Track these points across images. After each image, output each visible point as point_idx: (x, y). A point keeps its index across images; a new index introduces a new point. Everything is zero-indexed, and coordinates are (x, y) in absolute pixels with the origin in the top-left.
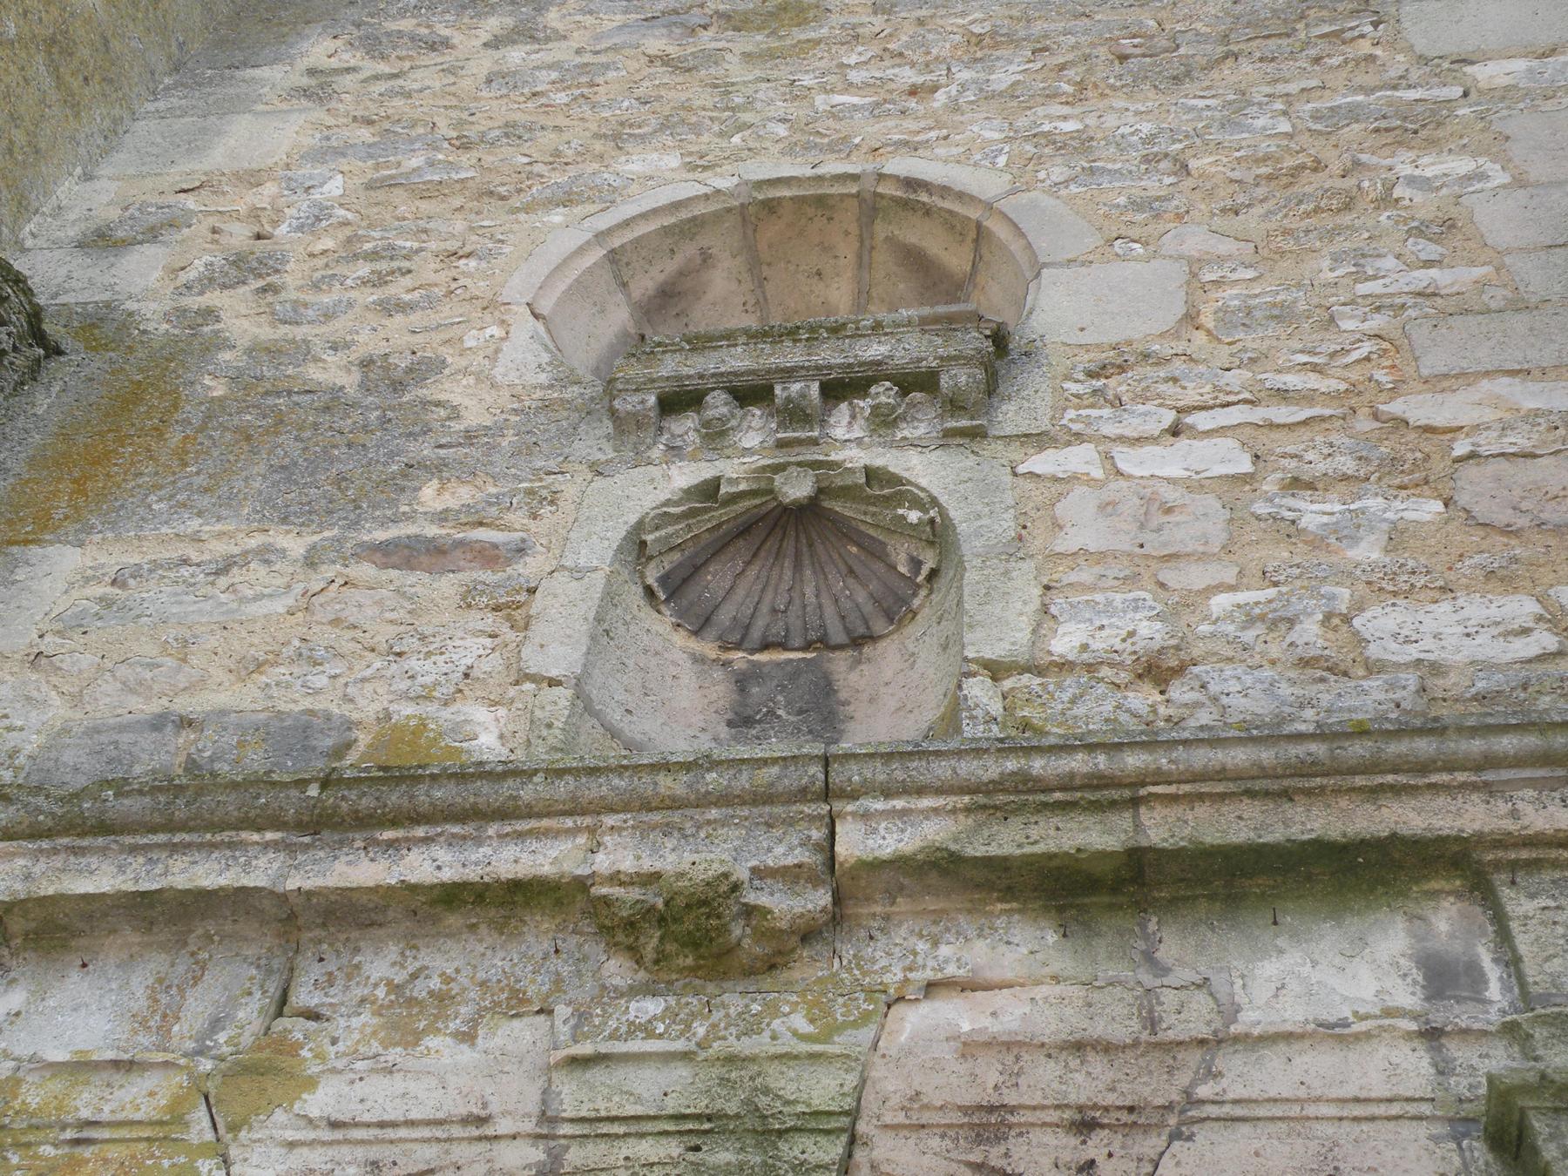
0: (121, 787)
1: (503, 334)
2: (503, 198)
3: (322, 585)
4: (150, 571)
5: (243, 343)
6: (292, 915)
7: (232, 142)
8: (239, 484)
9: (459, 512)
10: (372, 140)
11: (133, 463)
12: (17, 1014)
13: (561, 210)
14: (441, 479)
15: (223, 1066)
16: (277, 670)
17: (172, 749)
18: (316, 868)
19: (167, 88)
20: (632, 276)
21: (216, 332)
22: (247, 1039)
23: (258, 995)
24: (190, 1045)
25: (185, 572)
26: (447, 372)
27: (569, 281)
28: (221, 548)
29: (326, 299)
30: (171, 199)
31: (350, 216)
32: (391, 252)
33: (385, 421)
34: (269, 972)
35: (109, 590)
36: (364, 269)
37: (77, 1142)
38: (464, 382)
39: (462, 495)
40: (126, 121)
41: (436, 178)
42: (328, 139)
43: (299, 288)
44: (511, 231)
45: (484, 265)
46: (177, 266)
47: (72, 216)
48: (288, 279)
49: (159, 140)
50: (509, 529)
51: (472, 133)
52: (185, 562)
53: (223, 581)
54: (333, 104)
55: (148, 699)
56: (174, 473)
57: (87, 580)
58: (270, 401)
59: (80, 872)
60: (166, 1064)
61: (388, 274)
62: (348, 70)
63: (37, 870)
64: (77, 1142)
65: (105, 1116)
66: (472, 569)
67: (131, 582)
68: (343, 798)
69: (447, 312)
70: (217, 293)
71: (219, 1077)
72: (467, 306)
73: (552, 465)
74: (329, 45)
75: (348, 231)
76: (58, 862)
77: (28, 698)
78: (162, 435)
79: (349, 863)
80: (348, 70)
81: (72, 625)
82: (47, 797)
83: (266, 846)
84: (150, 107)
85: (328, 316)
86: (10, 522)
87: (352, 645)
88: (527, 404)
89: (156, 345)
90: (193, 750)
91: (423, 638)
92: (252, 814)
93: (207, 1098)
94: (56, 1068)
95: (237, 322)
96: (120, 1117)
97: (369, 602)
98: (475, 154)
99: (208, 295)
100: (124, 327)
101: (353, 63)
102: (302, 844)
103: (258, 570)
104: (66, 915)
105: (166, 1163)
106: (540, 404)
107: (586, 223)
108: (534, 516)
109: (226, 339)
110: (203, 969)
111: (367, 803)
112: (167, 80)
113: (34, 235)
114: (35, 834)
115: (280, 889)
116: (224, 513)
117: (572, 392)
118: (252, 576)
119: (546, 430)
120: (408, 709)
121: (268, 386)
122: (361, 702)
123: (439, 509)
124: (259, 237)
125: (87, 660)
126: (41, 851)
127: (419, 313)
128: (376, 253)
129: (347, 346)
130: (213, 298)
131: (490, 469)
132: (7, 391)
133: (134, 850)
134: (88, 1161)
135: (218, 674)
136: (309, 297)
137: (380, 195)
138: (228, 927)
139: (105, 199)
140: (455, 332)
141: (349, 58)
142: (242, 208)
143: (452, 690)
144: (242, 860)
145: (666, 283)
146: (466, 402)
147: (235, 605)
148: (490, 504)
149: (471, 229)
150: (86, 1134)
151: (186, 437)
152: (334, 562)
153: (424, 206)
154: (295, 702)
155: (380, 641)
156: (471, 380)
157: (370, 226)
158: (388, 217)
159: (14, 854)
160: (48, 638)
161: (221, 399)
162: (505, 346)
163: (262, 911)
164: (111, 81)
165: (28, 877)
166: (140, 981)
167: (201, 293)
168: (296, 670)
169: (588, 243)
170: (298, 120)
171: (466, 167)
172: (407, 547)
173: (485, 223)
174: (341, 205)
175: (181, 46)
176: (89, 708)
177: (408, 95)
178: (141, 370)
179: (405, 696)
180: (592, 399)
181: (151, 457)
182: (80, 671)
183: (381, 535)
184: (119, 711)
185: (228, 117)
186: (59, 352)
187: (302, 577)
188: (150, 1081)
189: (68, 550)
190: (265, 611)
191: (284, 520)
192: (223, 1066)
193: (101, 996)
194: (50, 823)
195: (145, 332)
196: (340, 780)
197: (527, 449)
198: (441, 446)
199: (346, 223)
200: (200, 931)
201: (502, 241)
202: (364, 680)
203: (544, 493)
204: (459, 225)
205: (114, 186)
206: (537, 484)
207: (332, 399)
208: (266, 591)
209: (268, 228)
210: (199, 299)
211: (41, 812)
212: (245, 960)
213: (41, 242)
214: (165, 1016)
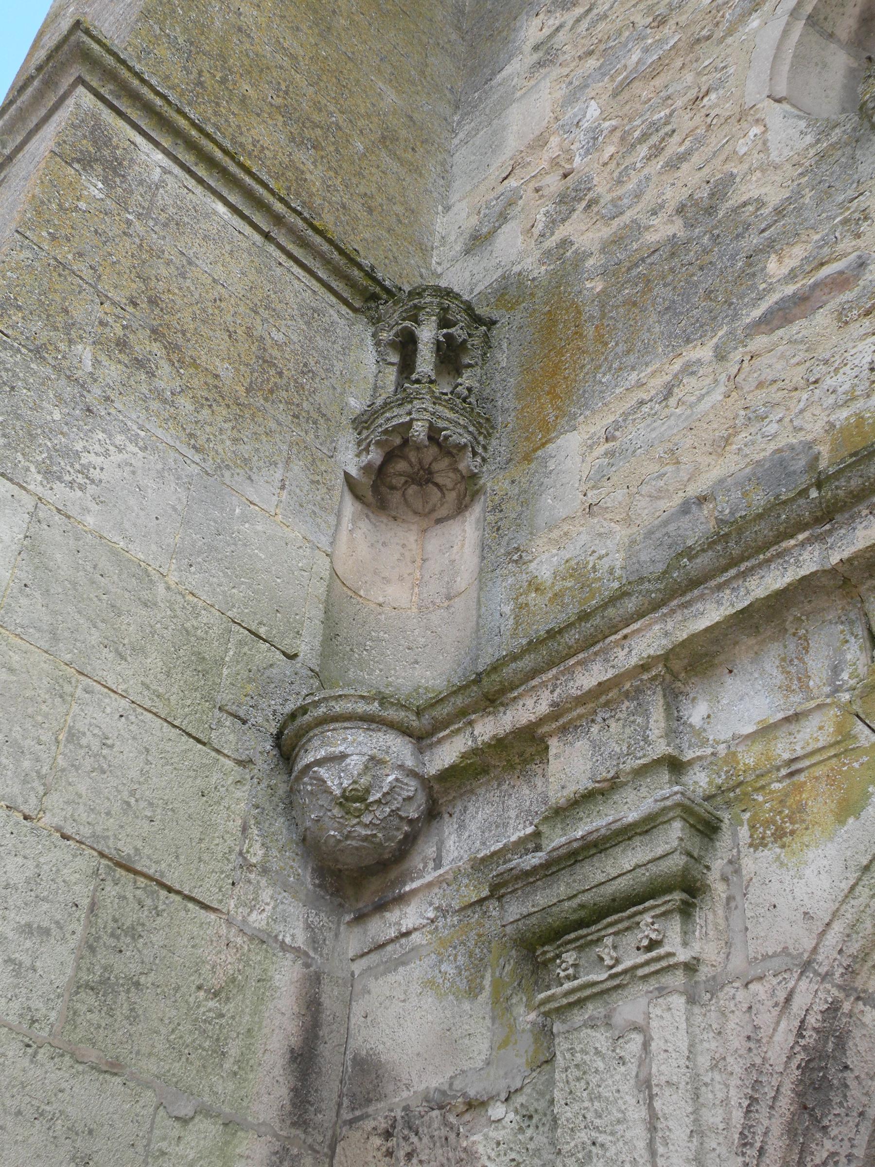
0: (689, 553)
1: (762, 129)
2: (708, 38)
3: (737, 367)
4: (624, 420)
5: (595, 248)
6: (846, 580)
7: (515, 127)
8: (646, 336)
9: (801, 266)
10: (599, 64)
11: (575, 362)
12: (709, 716)
13: (754, 15)
14: (776, 252)
15: (857, 692)
16: (740, 437)
17: (703, 520)
18: (845, 542)
19: (459, 123)
20: (834, 25)
21: (576, 252)
22: (862, 670)
23: (853, 640)
24: (827, 689)
25: (645, 409)
26: (738, 179)
27: (788, 61)
28: (658, 382)
29: (630, 186)
30: (500, 189)
31: (613, 122)
32: (655, 127)
33: (715, 239)
34: (851, 623)
35: (607, 446)
36: (643, 150)
37: (791, 774)
38: (754, 179)
39: (797, 254)
40: (448, 160)
41: (655, 57)
42: (571, 83)
43: (610, 190)
44: (728, 56)
45: (721, 92)
46: (529, 226)
47: (453, 238)
48: (599, 189)
49: (473, 158)
50: (845, 255)
51: (661, 10)
52: (642, 403)
53: (672, 401)
54: (561, 58)
55: (670, 498)
56: (603, 353)
57: (591, 447)
58: (634, 272)
59: (695, 616)
60: (819, 707)
61: (661, 143)
62: (558, 30)
63: (669, 626)
64: (791, 774)
65: (799, 753)
66: (833, 298)
67: (617, 434)
68: (837, 488)
69: (714, 141)
70: (562, 227)
71: (858, 700)
72: (726, 128)
73: (851, 193)
74: (536, 22)
75: (618, 134)
76: (678, 616)
77: (600, 535)
78: (581, 335)
79: (866, 528)
80: (558, 30)
81: (599, 478)
82: (649, 581)
83: (802, 544)
84: (456, 141)
85: (638, 195)
86: (527, 439)
87: (780, 394)
88: (807, 164)
89: (545, 283)
90: (716, 514)
91: (826, 362)
92: (782, 529)
93: (858, 716)
94: (751, 737)
95: (585, 237)
96: (809, 749)
97: (775, 360)
98: (672, 22)
99: (557, 232)
100: (520, 283)
101: (557, 23)
102: (826, 531)
103: (690, 382)
104: (702, 646)
105: (856, 765)
106: (817, 158)
107: (779, 11)
108: (858, 236)
109: (584, 251)
110: (806, 640)
111: (855, 483)
112: (456, 118)
113: (439, 264)
114: (655, 607)
115: (828, 567)
116: (648, 359)
117: (836, 135)
118: (688, 388)
119: (832, 173)
120: (844, 413)
121: (627, 264)
122: (808, 427)
123: (787, 272)
124: (565, 176)
125: (620, 494)
126: (665, 615)
127: (696, 154)
128: (645, 134)
129: (662, 206)
130: (561, 232)
131: (806, 224)
132: (480, 363)
133: (720, 588)
134: (805, 783)
135: (704, 460)
136: (619, 192)
137: (625, 95)
138: (808, 608)
139: (464, 215)
140: (728, 149)
141: (553, 22)
142: (545, 165)
143: (867, 384)
144: (792, 560)
145: (862, 12)
146: (763, 191)
147: (689, 411)
148: (821, 247)
149: (699, 74)
150: (794, 767)
151: (597, 327)
152: (736, 348)
153: (658, 82)
154: (764, 450)
155: (798, 380)
156: (758, 174)
157: (630, 120)
158: (638, 106)
159: (650, 625)
160: (589, 494)
161: (602, 291)
162: (769, 136)
163: (824, 586)
164: (426, 141)
165: (666, 634)
166: (771, 665)
167: (552, 234)
168: (753, 430)
169: (788, 24)
170: (546, 84)
171: (671, 35)
172: (780, 309)
173: (706, 63)
174: (604, 120)
175: (451, 90)
176: (638, 522)
177: (606, 16)
178: (546, 304)
179: (837, 406)
180: (854, 129)
181: (583, 352)
182: (620, 503)
183: (757, 313)
184: (657, 514)
185: (503, 115)
186: (494, 323)
187: (721, 370)
188: (815, 721)
189: (569, 435)
190: (710, 404)
191: (688, 341)
192: (857, 692)
193: (752, 685)
194: (661, 596)
195: (534, 279)
196: (829, 478)
197: (825, 194)
198: (763, 231)
199: (614, 129)
200: (791, 618)
201: (725, 67)
202: (802, 411)
203: (856, 215)
204: (689, 77)
205: (464, 204)
206: (847, 214)
207: (673, 247)
208: (703, 392)
209: (568, 166)
210: (553, 238)
211: (652, 592)
212: (831, 623)
213: (446, 265)
214: (799, 679)
